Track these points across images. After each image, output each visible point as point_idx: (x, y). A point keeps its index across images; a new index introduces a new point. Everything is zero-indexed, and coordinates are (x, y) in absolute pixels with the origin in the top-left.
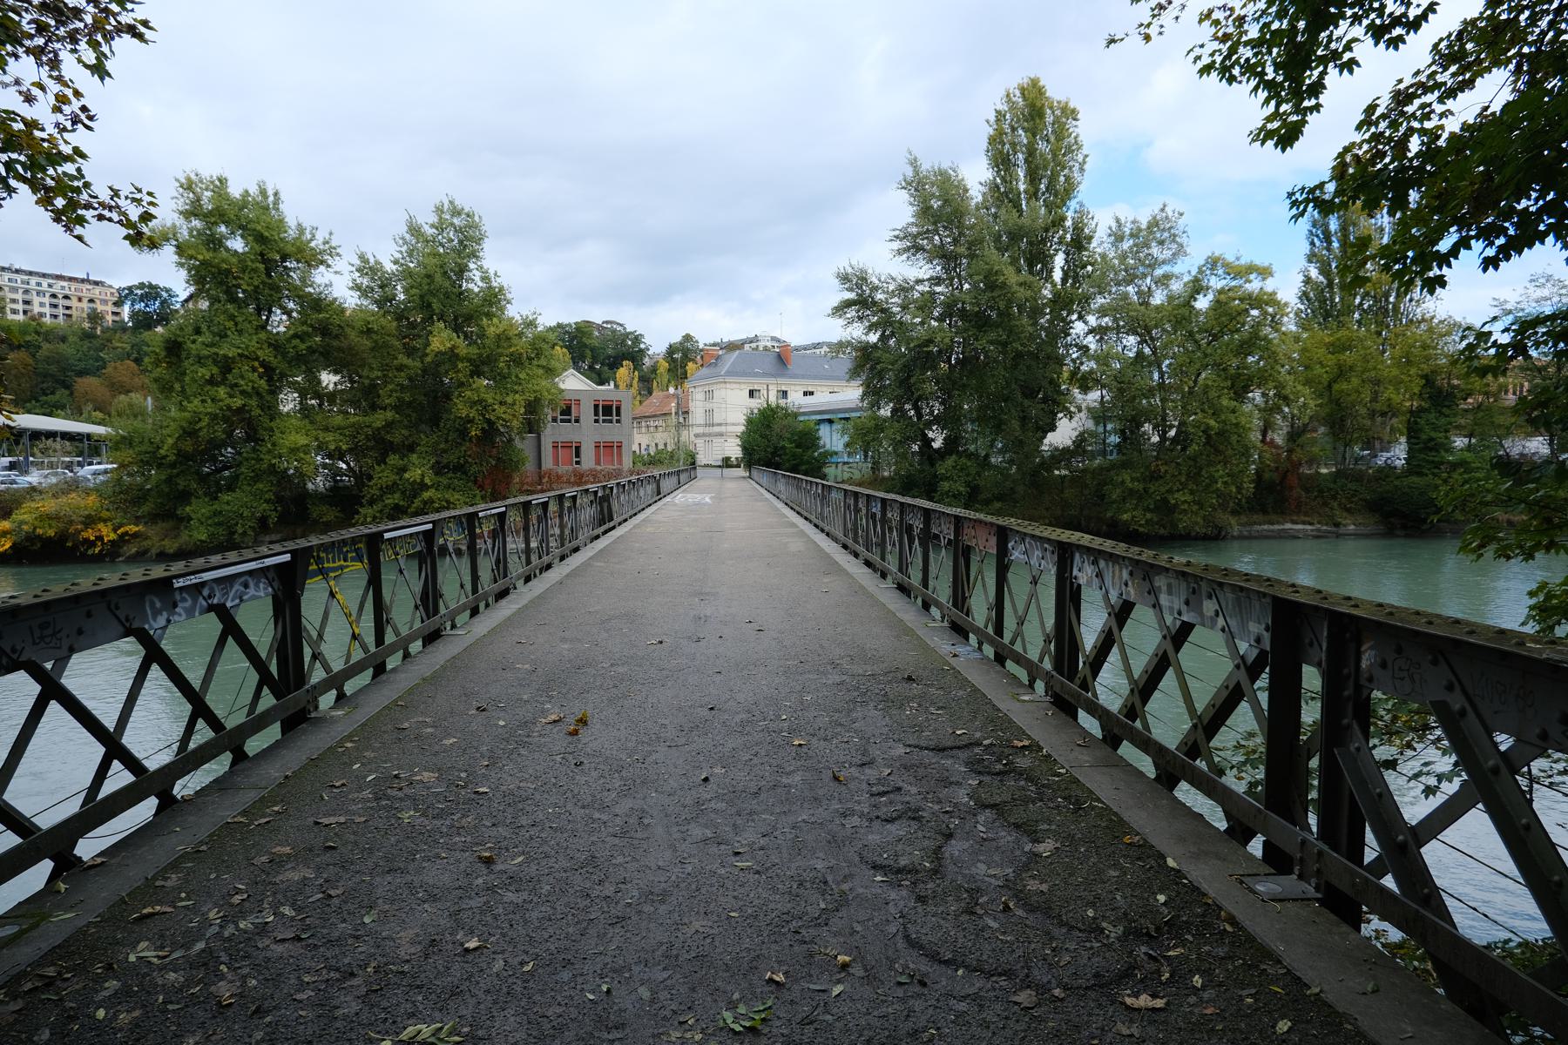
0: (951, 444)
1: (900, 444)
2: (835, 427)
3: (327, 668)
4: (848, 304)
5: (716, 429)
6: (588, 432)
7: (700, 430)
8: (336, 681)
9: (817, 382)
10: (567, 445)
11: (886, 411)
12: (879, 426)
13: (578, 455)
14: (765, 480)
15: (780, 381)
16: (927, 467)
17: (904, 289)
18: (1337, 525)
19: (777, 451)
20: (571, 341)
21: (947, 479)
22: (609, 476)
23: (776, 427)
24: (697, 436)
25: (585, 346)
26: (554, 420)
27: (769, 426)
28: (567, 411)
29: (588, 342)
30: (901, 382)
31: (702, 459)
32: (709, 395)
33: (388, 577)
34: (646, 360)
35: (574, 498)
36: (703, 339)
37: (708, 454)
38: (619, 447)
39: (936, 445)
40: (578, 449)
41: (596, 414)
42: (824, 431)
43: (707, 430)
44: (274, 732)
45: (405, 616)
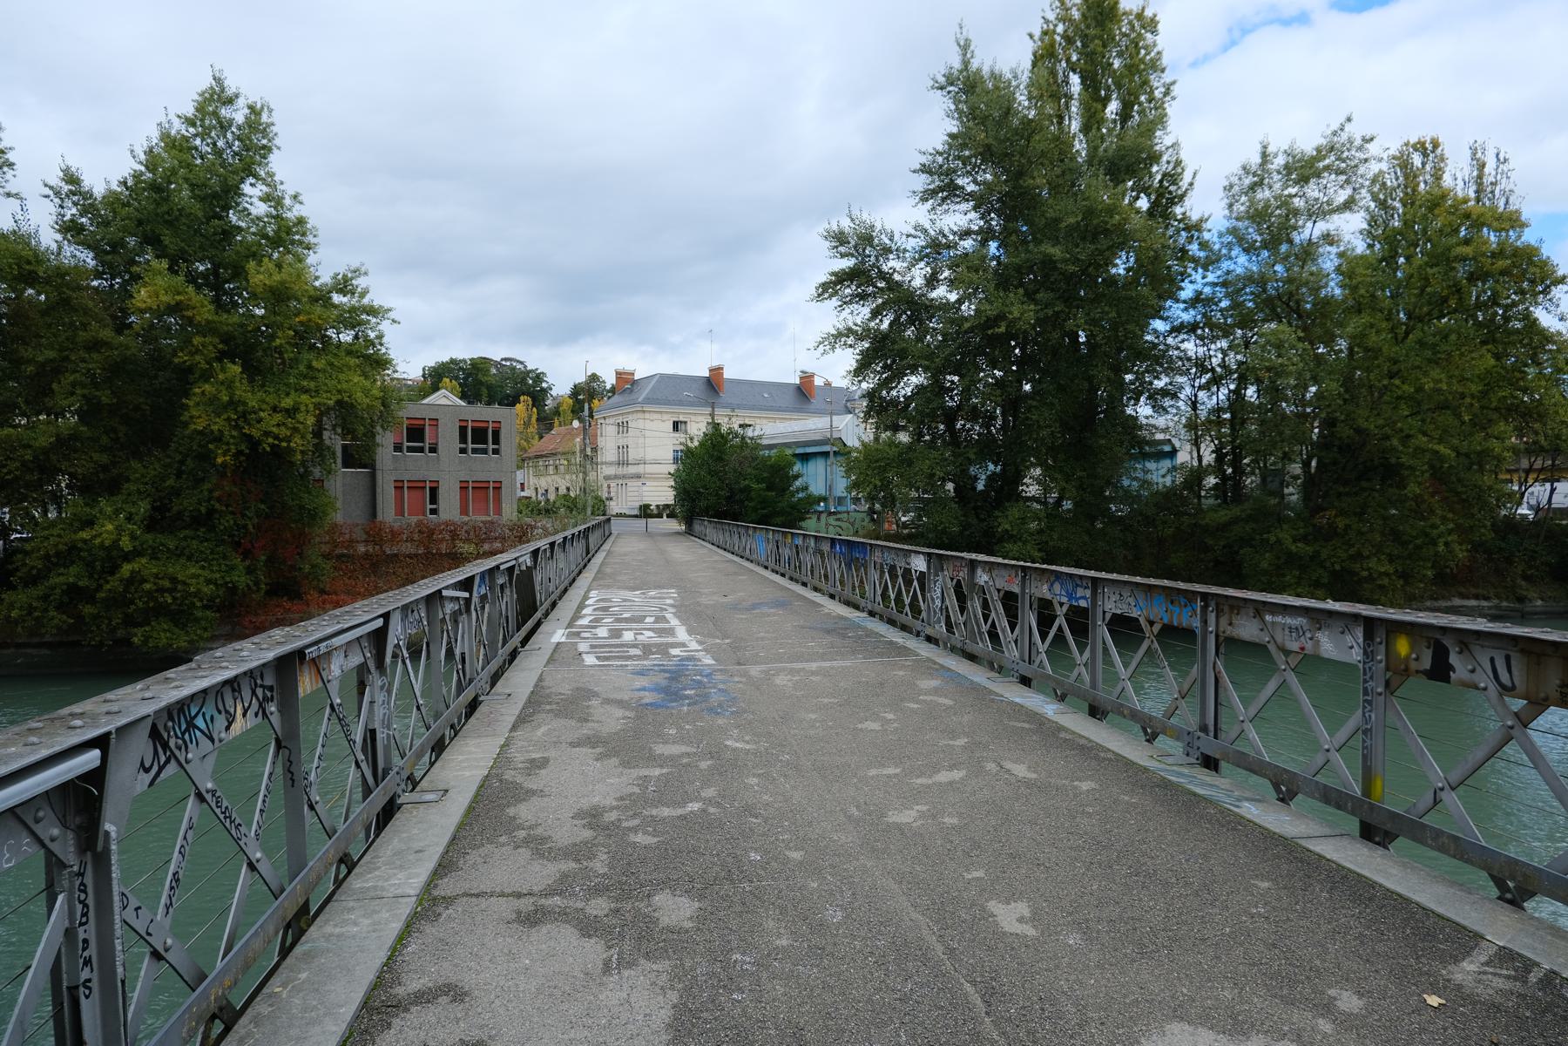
4: (841, 278)
5: (632, 470)
7: (611, 471)
10: (416, 486)
12: (905, 458)
13: (434, 500)
14: (719, 537)
17: (935, 248)
18: (1521, 600)
20: (465, 379)
24: (607, 478)
25: (481, 383)
26: (398, 448)
27: (720, 459)
28: (416, 432)
31: (614, 507)
32: (623, 427)
38: (498, 489)
40: (434, 492)
41: (463, 439)
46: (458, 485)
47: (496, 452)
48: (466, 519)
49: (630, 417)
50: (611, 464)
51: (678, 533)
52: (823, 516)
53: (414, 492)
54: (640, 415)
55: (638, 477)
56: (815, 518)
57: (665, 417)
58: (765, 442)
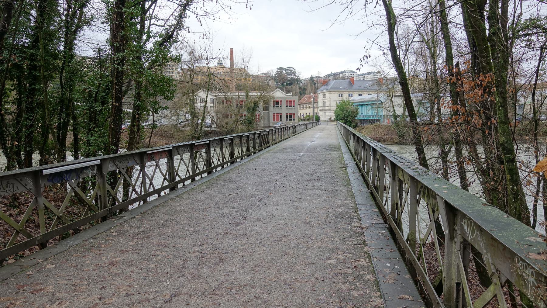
3: (199, 170)
8: (183, 181)
9: (363, 90)
10: (277, 115)
24: (320, 110)
28: (277, 103)
32: (325, 96)
33: (224, 149)
37: (325, 116)
43: (324, 108)
44: (167, 191)
45: (201, 166)
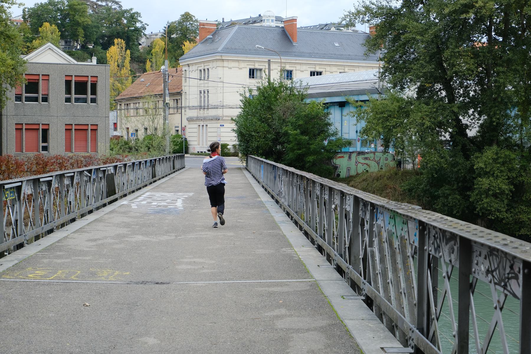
0: (491, 133)
1: (427, 133)
2: (346, 110)
5: (212, 113)
6: (58, 113)
7: (193, 113)
9: (325, 61)
10: (32, 128)
11: (410, 92)
12: (404, 109)
13: (45, 139)
14: (261, 175)
15: (284, 59)
16: (460, 160)
19: (279, 137)
20: (63, 19)
21: (487, 174)
22: (78, 163)
23: (278, 109)
24: (190, 120)
25: (78, 24)
26: (18, 98)
27: (269, 108)
28: (32, 86)
29: (81, 20)
30: (432, 57)
34: (143, 40)
35: (72, 178)
36: (205, 14)
38: (94, 131)
39: (471, 133)
40: (45, 132)
41: (68, 91)
42: (335, 116)
46: (64, 128)
47: (93, 101)
48: (70, 154)
49: (210, 65)
50: (194, 108)
51: (240, 169)
52: (354, 156)
53: (79, 132)
54: (220, 63)
55: (217, 119)
56: (346, 157)
57: (243, 65)
58: (310, 92)
